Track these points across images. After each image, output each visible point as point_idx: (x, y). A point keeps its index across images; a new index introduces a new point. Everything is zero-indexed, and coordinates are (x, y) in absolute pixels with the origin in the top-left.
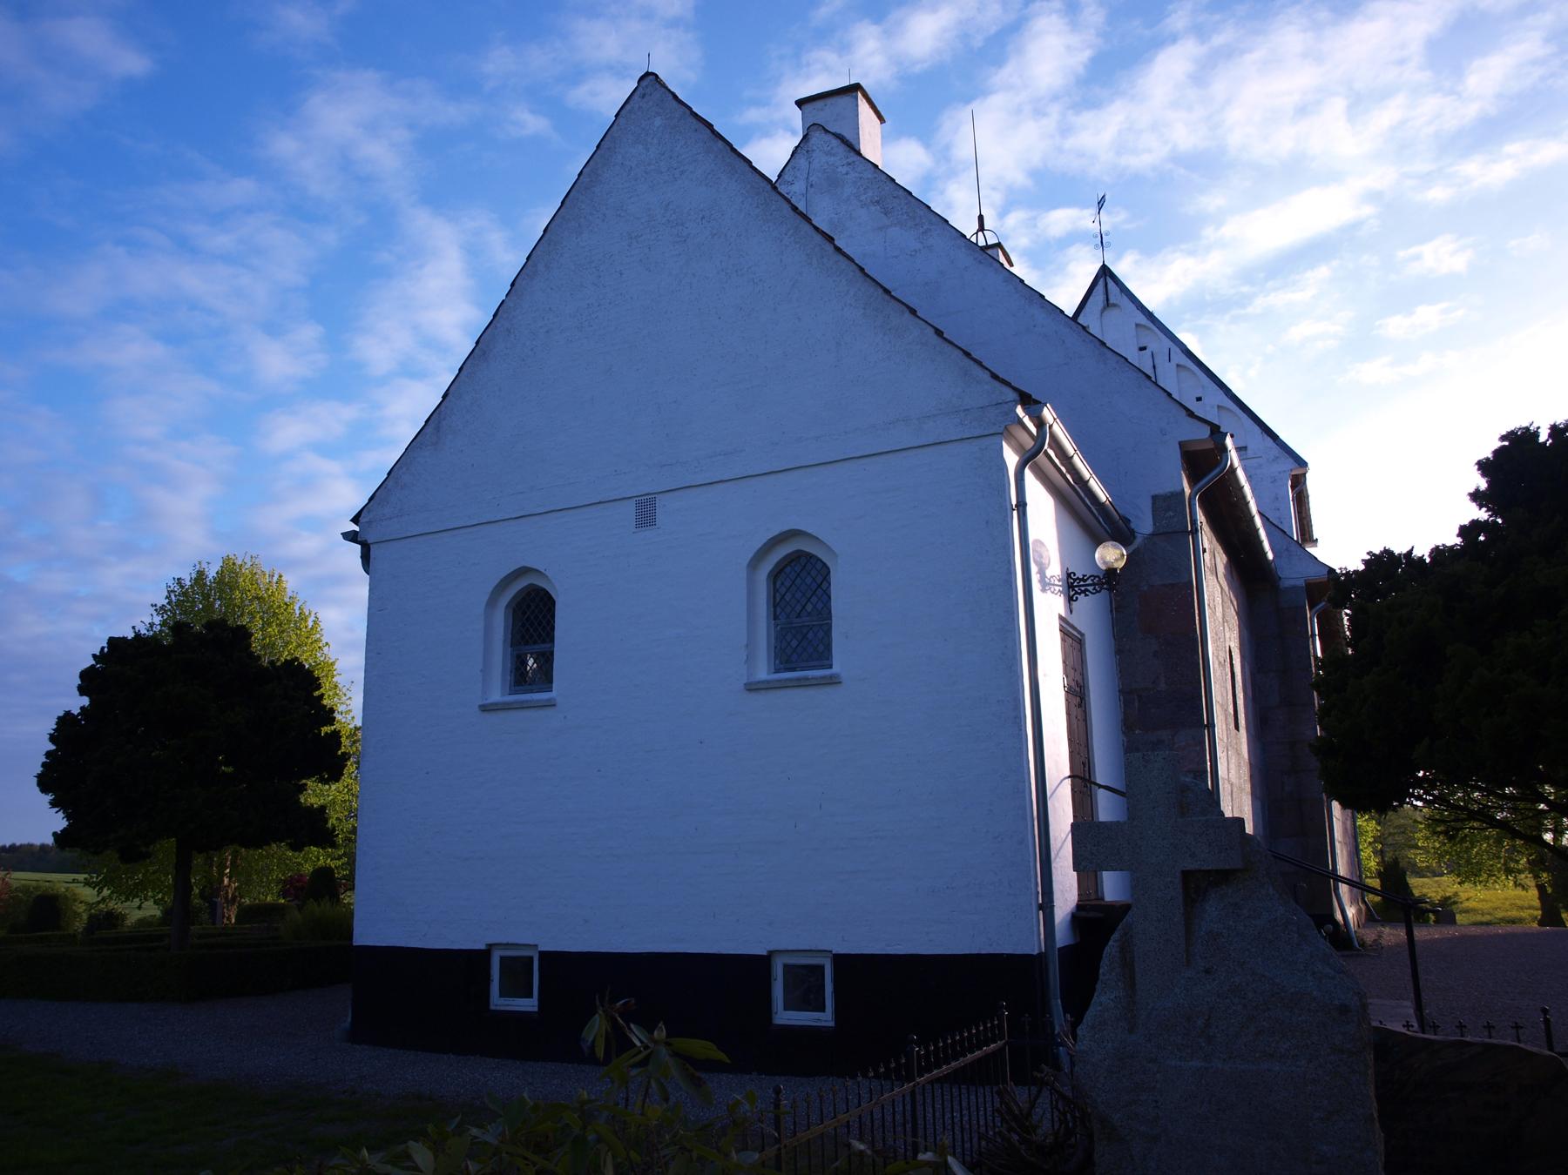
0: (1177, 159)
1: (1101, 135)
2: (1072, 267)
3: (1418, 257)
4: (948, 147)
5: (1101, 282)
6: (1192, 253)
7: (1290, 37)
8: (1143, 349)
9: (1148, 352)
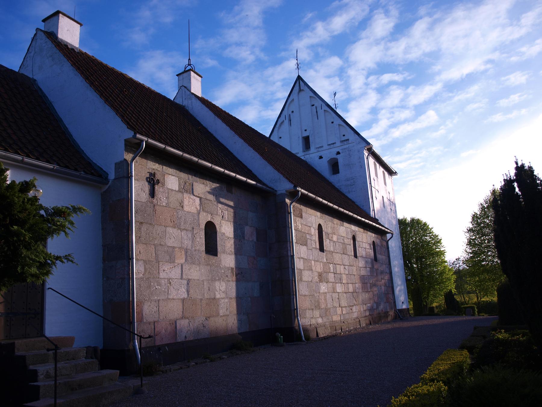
0: (426, 55)
1: (399, 50)
2: (391, 93)
3: (508, 79)
4: (348, 58)
5: (298, 82)
6: (431, 85)
7: (459, 13)
8: (313, 105)
9: (315, 106)
